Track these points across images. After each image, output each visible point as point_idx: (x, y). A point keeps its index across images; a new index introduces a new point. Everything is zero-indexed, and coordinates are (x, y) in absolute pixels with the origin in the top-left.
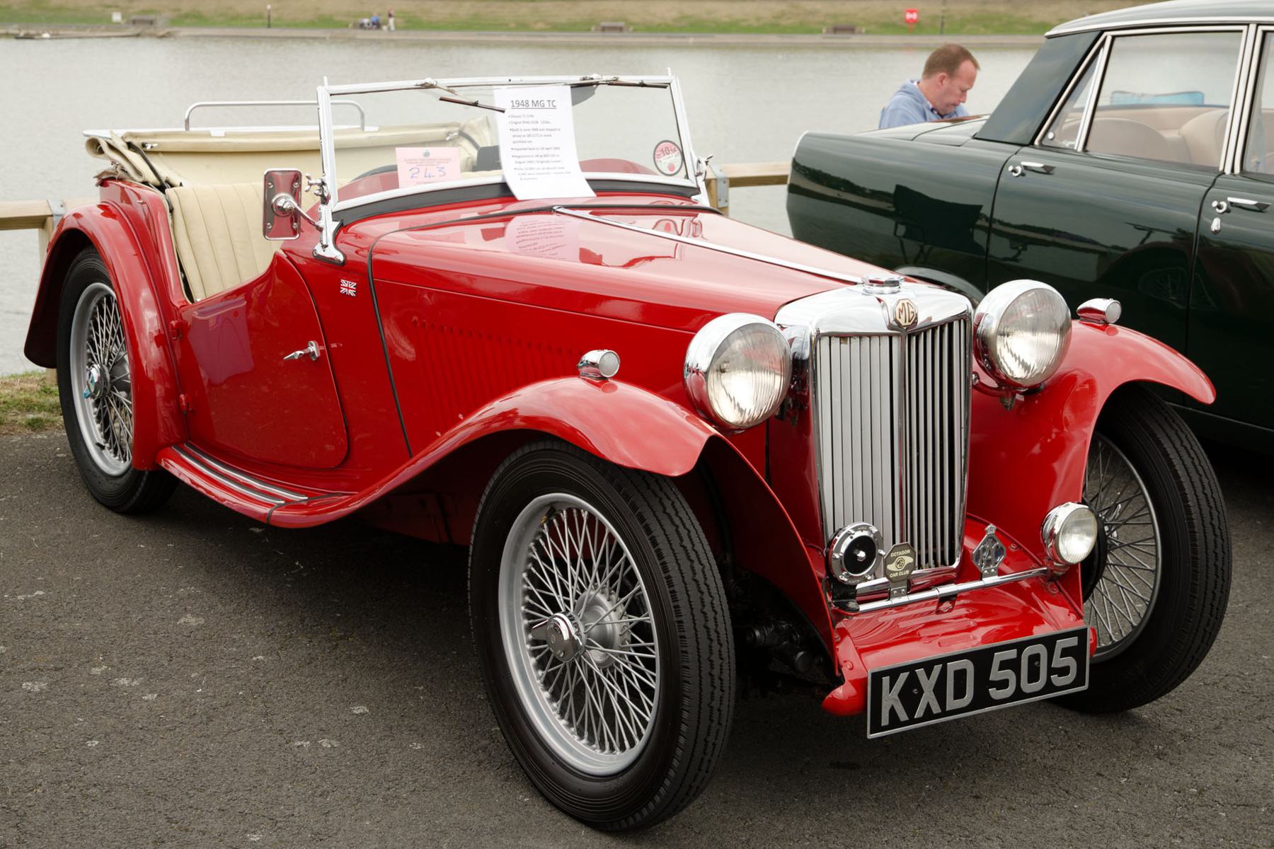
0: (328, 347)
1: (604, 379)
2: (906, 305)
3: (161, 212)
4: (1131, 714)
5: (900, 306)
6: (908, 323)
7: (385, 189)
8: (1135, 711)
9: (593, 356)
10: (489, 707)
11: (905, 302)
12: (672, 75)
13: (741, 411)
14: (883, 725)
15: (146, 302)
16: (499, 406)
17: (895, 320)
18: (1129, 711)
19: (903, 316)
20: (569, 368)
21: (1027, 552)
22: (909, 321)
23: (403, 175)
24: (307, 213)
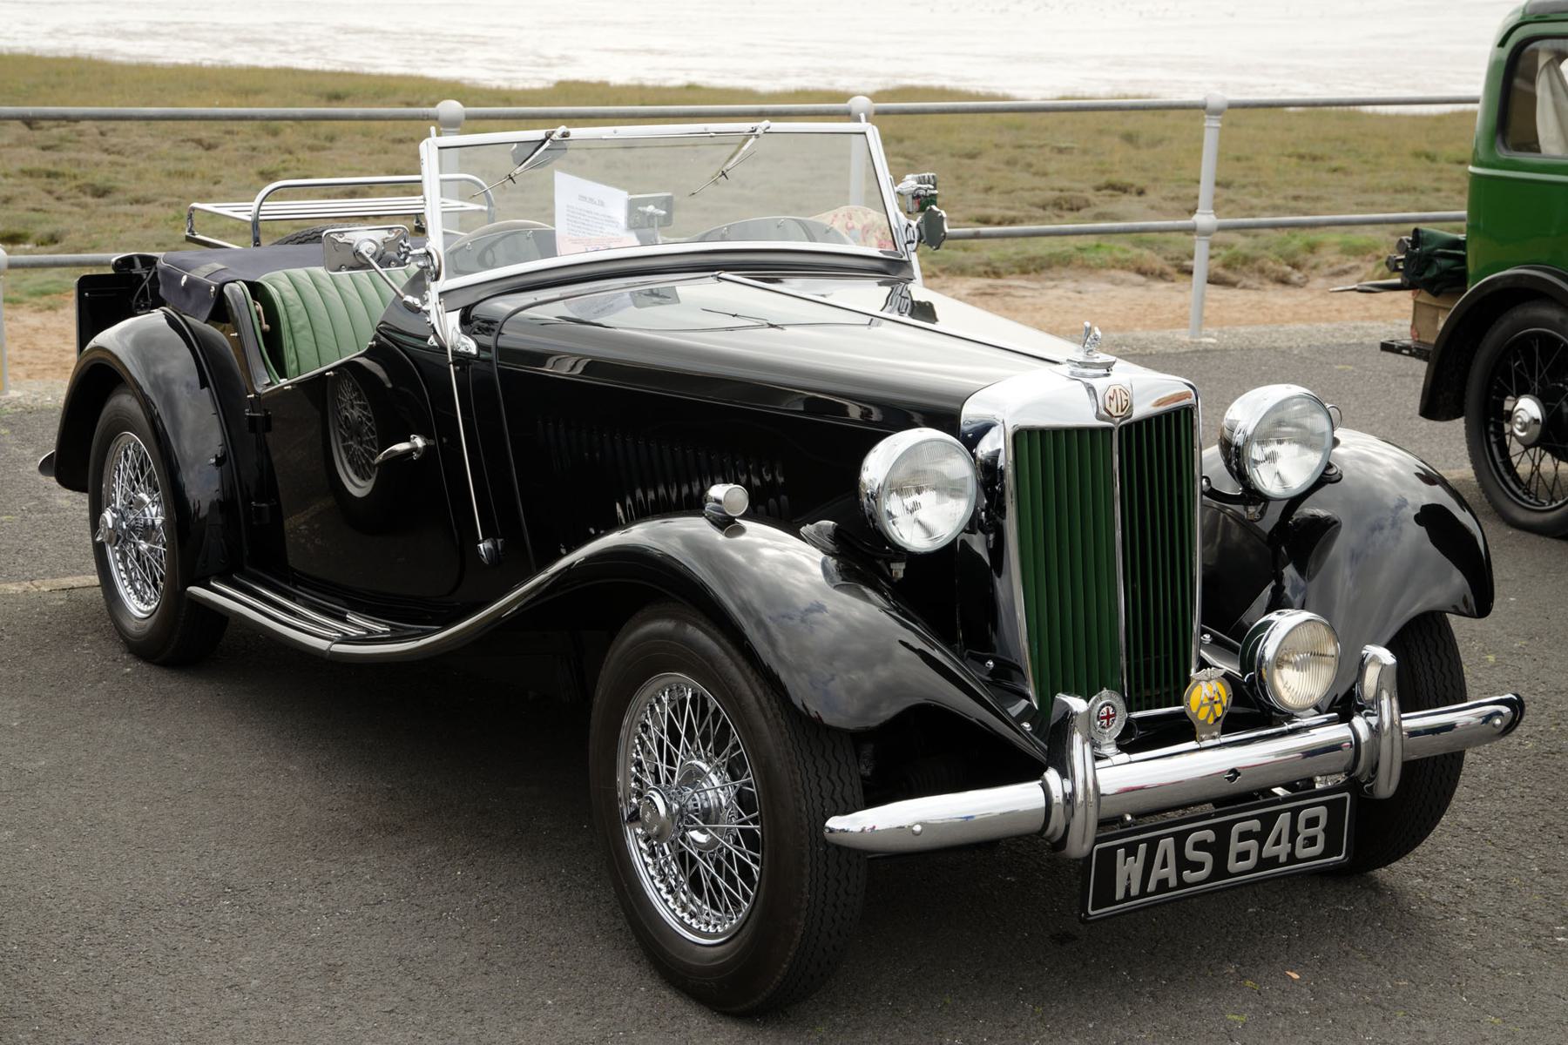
0: (440, 441)
1: (731, 520)
2: (1118, 391)
3: (164, 286)
4: (1372, 877)
5: (1110, 393)
6: (1120, 413)
7: (543, 257)
8: (1381, 873)
9: (718, 491)
10: (1238, 315)
11: (1117, 388)
12: (143, 267)
13: (929, 532)
14: (1145, 845)
15: (292, 363)
16: (638, 534)
17: (1105, 409)
18: (1371, 873)
19: (1114, 403)
20: (694, 505)
21: (1426, 211)
22: (1122, 411)
23: (562, 244)
24: (402, 290)
